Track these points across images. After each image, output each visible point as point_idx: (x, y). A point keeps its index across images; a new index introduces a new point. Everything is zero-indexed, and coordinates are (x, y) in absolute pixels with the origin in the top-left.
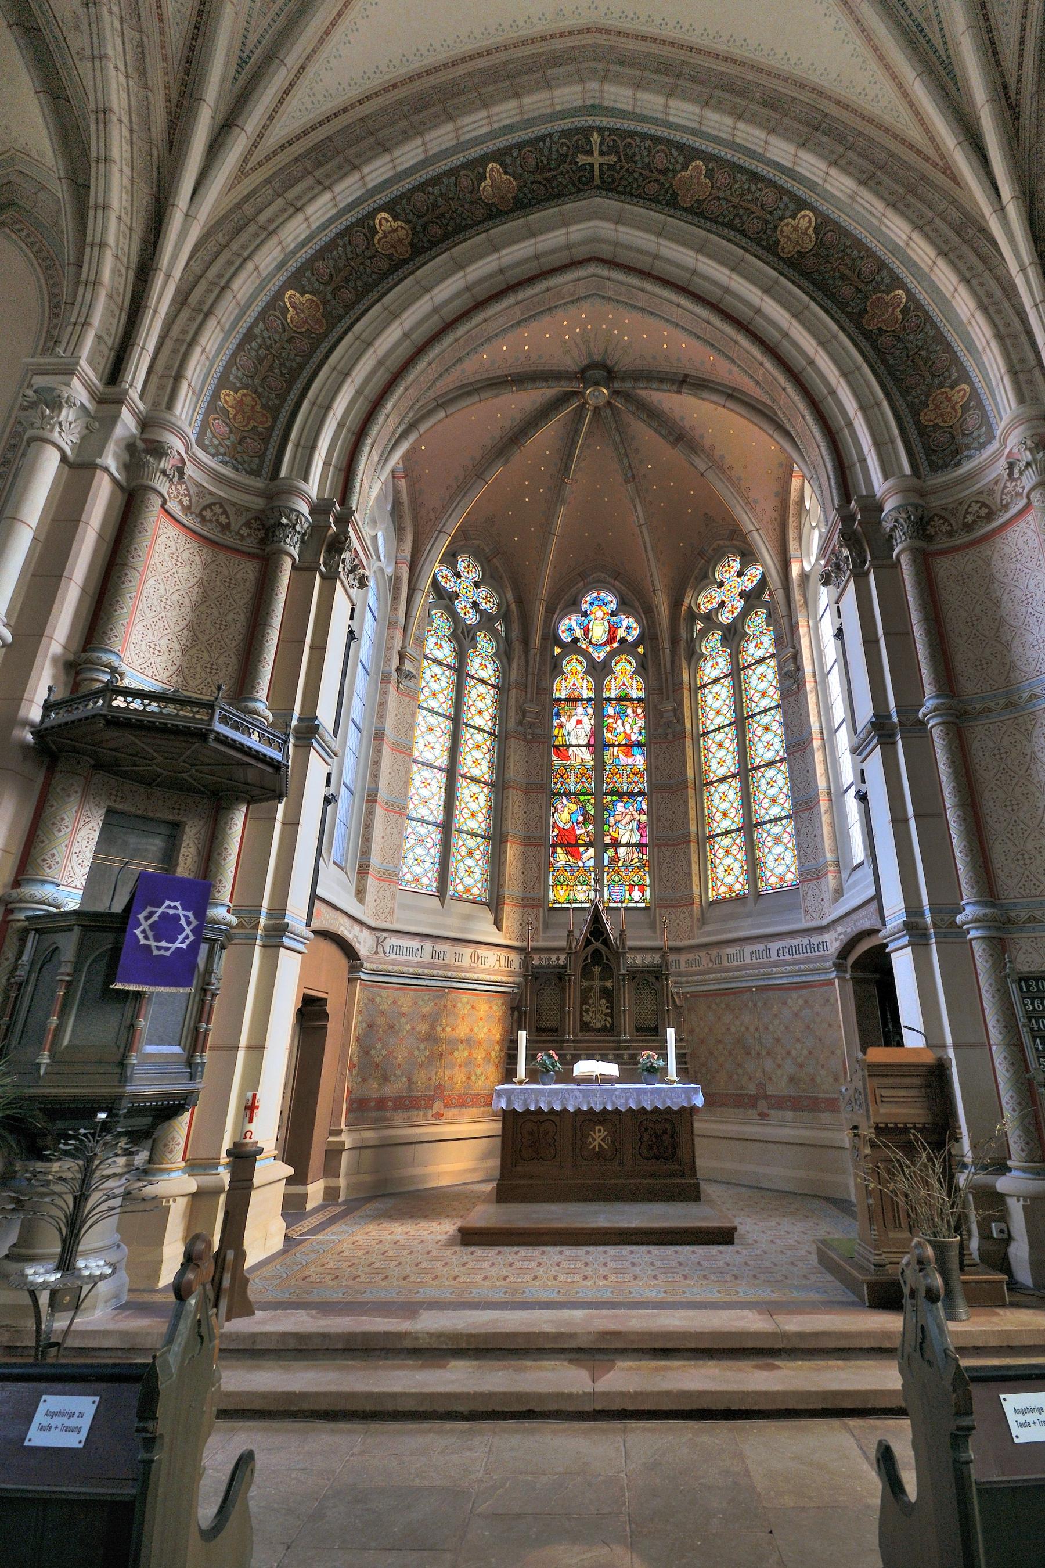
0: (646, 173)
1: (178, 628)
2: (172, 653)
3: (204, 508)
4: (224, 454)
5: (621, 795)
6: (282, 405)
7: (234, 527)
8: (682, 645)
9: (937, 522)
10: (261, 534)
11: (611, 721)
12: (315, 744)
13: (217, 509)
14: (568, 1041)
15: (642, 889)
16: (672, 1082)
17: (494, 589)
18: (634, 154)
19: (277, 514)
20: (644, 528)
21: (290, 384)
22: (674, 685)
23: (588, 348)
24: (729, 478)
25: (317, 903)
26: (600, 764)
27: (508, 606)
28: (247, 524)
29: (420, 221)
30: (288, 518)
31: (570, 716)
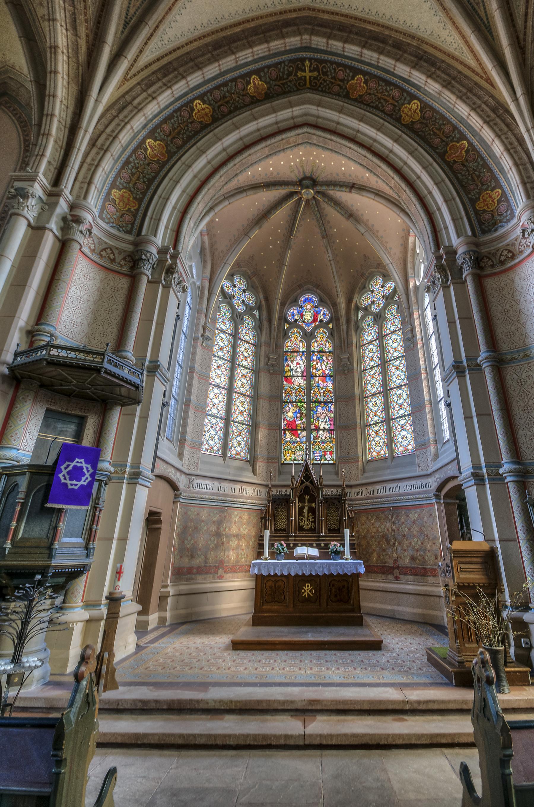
0: (334, 81)
1: (87, 313)
2: (83, 326)
3: (102, 251)
4: (113, 223)
5: (320, 403)
6: (143, 197)
7: (117, 260)
8: (353, 323)
9: (486, 260)
10: (131, 264)
11: (315, 363)
12: (158, 375)
13: (109, 251)
14: (292, 536)
15: (331, 453)
16: (347, 559)
17: (253, 293)
18: (327, 71)
19: (140, 253)
20: (332, 262)
21: (148, 187)
22: (348, 345)
23: (303, 169)
24: (377, 237)
25: (157, 460)
26: (309, 387)
27: (261, 302)
28: (124, 259)
29: (217, 105)
30: (146, 256)
31: (293, 360)
